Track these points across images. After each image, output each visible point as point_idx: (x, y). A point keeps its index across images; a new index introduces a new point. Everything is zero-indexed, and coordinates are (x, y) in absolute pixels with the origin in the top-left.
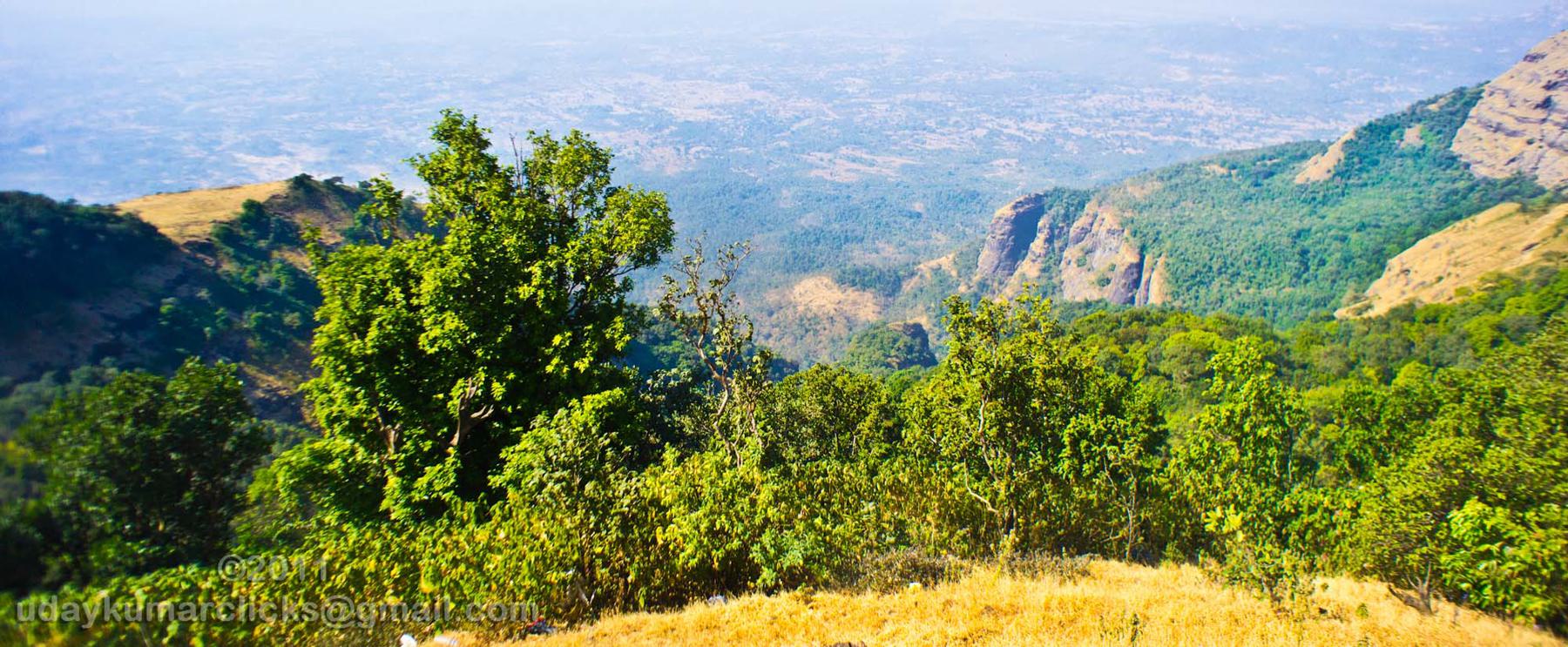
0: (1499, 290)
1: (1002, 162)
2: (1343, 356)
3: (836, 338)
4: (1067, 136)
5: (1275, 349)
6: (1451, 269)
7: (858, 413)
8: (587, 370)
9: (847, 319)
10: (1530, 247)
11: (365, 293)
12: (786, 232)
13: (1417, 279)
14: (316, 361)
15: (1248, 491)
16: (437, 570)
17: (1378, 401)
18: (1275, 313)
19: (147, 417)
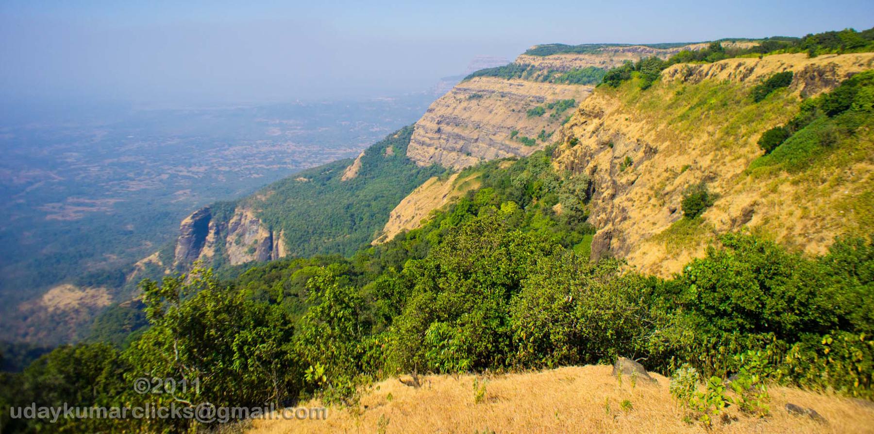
0: (437, 218)
1: (181, 192)
2: (379, 264)
4: (218, 172)
5: (347, 268)
6: (417, 212)
9: (89, 308)
10: (445, 196)
13: (404, 219)
15: (339, 348)
17: (392, 283)
18: (344, 249)
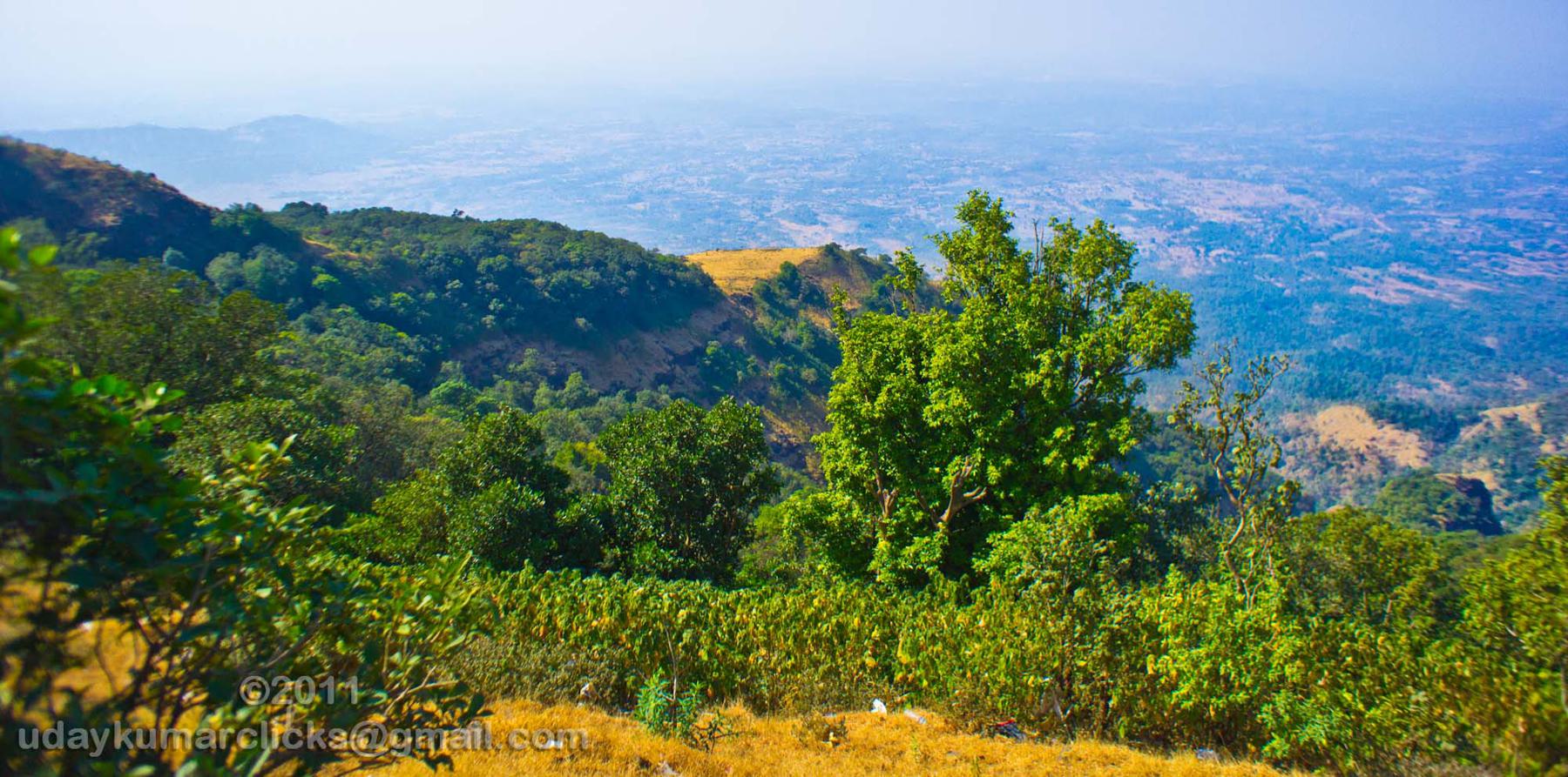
3: (1365, 479)
7: (1397, 573)
8: (1085, 469)
9: (1383, 460)
11: (879, 359)
12: (1314, 352)
14: (829, 416)
16: (915, 643)
19: (688, 443)
